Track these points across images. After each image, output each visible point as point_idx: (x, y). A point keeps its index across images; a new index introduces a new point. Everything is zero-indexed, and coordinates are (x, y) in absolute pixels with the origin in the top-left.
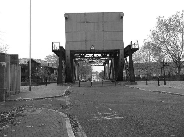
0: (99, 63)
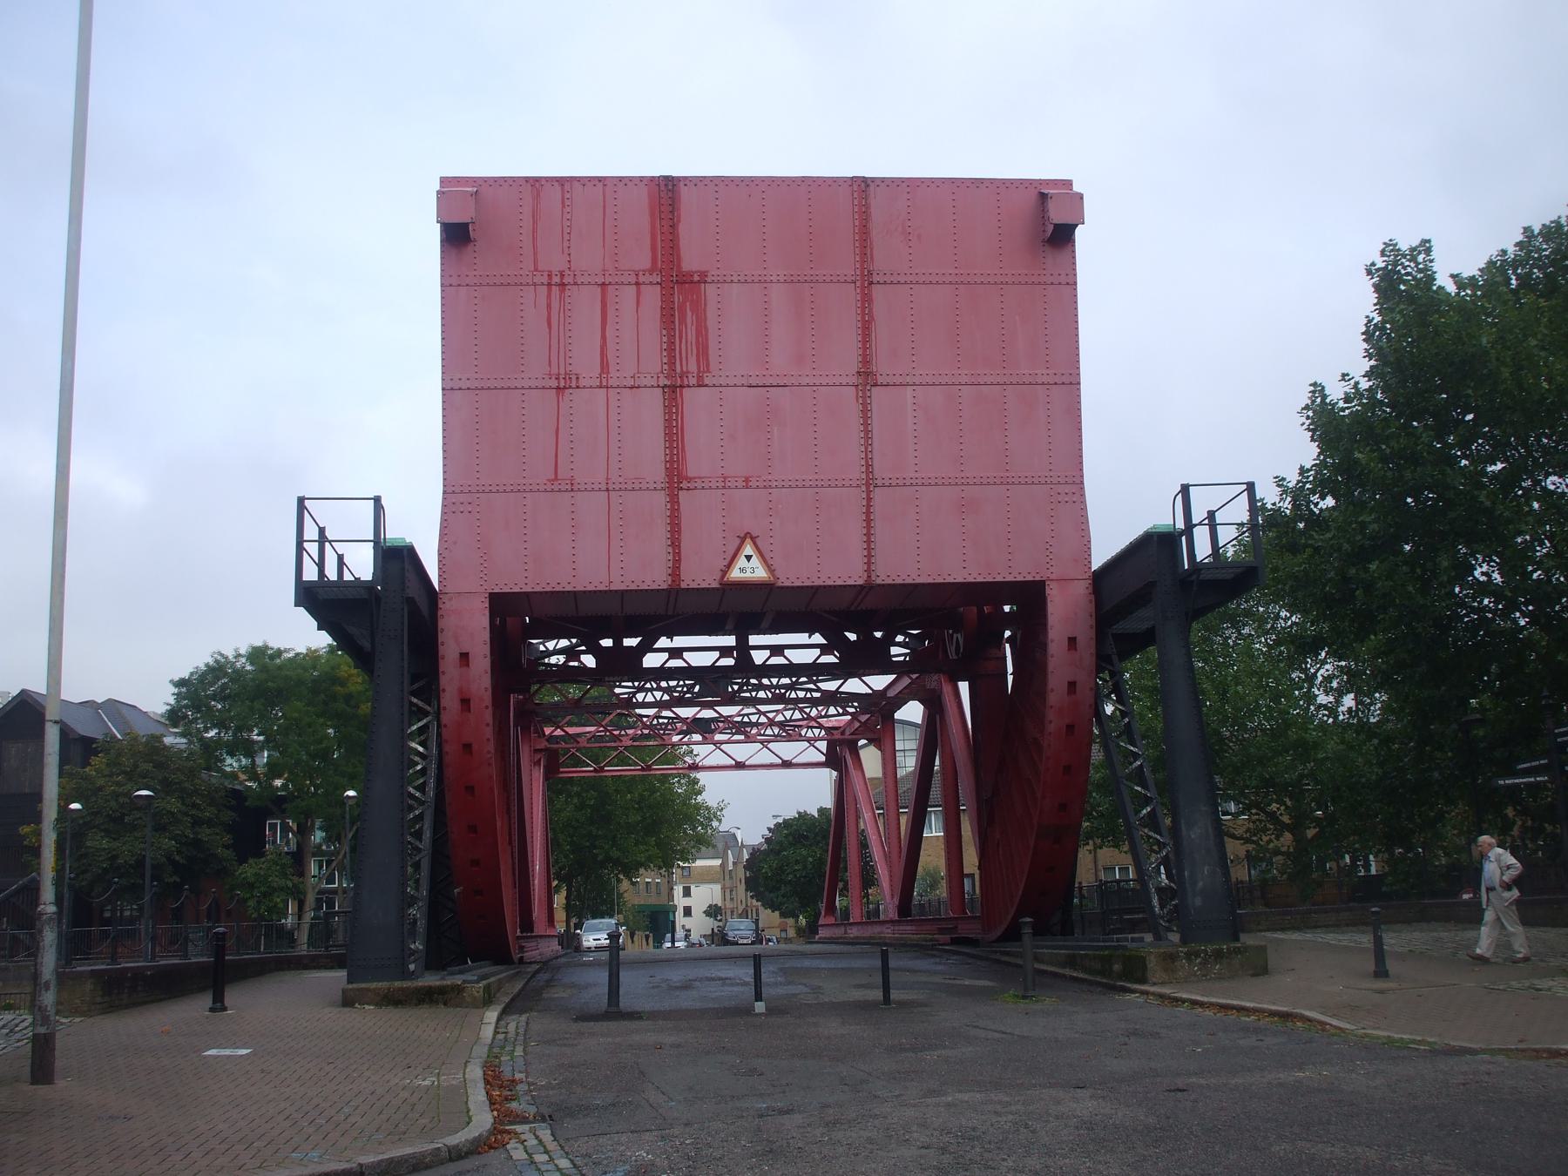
0: (789, 731)
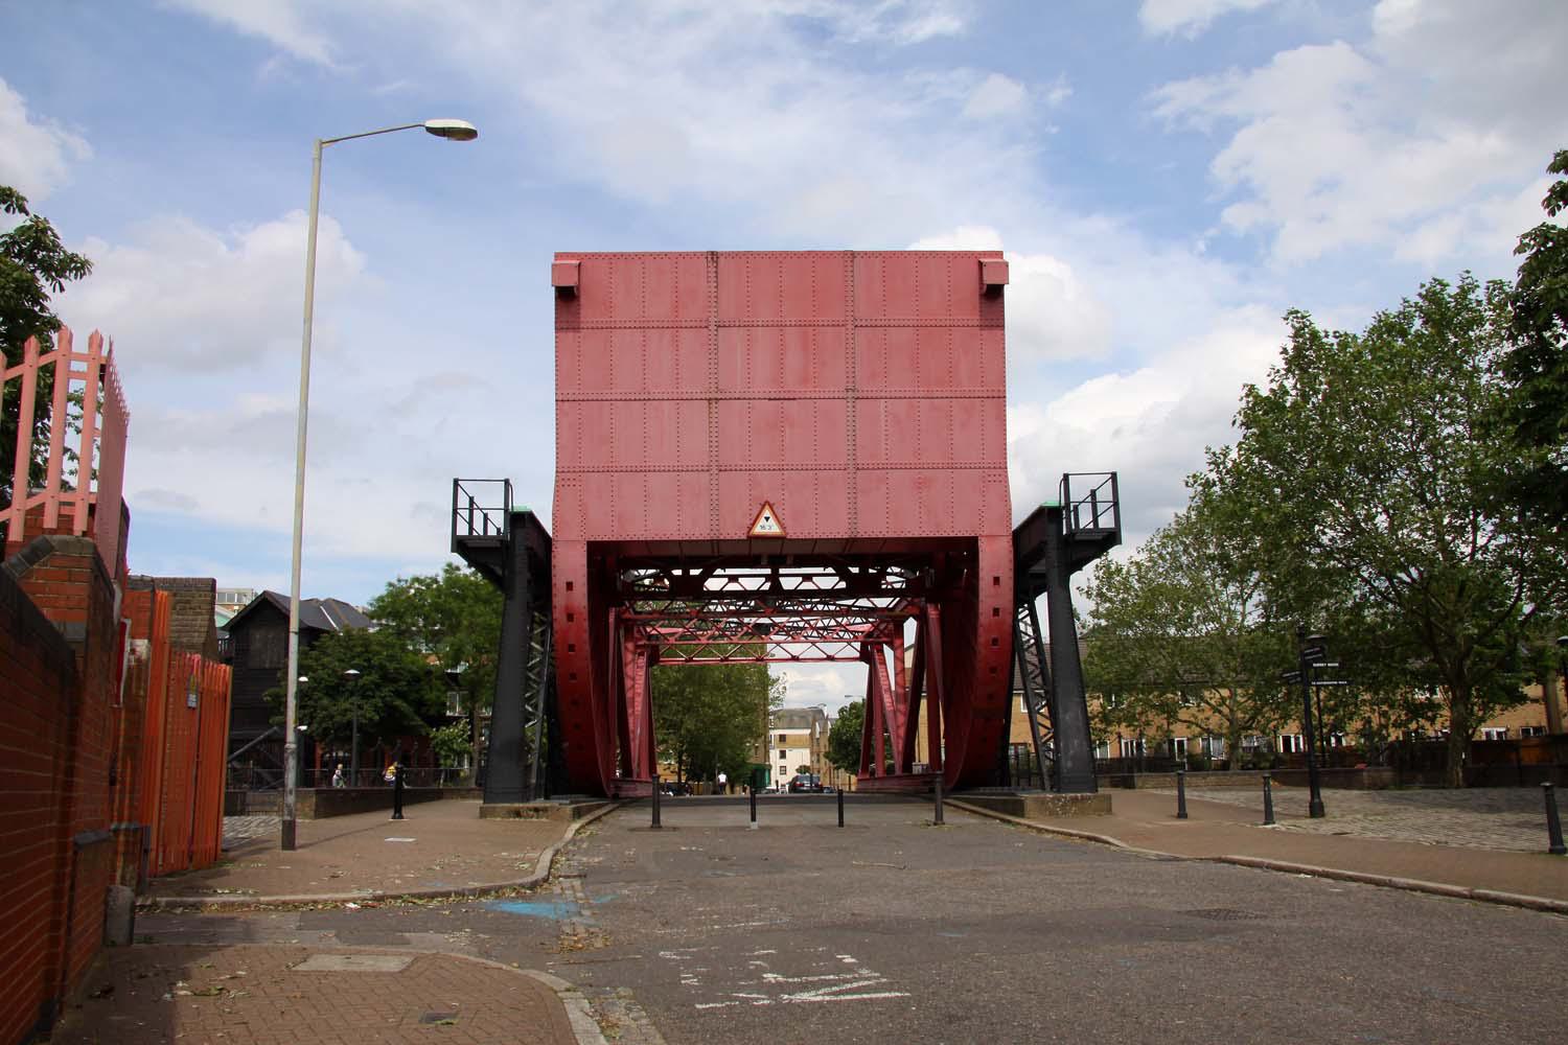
0: (825, 634)
